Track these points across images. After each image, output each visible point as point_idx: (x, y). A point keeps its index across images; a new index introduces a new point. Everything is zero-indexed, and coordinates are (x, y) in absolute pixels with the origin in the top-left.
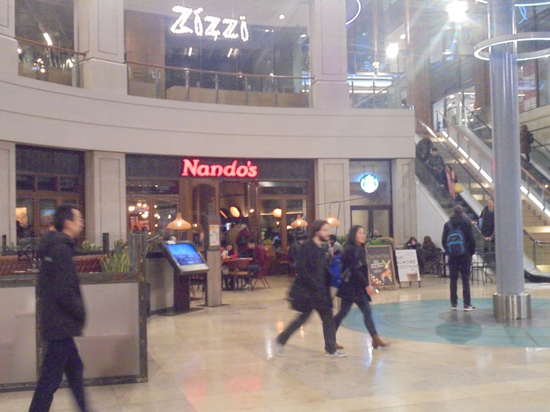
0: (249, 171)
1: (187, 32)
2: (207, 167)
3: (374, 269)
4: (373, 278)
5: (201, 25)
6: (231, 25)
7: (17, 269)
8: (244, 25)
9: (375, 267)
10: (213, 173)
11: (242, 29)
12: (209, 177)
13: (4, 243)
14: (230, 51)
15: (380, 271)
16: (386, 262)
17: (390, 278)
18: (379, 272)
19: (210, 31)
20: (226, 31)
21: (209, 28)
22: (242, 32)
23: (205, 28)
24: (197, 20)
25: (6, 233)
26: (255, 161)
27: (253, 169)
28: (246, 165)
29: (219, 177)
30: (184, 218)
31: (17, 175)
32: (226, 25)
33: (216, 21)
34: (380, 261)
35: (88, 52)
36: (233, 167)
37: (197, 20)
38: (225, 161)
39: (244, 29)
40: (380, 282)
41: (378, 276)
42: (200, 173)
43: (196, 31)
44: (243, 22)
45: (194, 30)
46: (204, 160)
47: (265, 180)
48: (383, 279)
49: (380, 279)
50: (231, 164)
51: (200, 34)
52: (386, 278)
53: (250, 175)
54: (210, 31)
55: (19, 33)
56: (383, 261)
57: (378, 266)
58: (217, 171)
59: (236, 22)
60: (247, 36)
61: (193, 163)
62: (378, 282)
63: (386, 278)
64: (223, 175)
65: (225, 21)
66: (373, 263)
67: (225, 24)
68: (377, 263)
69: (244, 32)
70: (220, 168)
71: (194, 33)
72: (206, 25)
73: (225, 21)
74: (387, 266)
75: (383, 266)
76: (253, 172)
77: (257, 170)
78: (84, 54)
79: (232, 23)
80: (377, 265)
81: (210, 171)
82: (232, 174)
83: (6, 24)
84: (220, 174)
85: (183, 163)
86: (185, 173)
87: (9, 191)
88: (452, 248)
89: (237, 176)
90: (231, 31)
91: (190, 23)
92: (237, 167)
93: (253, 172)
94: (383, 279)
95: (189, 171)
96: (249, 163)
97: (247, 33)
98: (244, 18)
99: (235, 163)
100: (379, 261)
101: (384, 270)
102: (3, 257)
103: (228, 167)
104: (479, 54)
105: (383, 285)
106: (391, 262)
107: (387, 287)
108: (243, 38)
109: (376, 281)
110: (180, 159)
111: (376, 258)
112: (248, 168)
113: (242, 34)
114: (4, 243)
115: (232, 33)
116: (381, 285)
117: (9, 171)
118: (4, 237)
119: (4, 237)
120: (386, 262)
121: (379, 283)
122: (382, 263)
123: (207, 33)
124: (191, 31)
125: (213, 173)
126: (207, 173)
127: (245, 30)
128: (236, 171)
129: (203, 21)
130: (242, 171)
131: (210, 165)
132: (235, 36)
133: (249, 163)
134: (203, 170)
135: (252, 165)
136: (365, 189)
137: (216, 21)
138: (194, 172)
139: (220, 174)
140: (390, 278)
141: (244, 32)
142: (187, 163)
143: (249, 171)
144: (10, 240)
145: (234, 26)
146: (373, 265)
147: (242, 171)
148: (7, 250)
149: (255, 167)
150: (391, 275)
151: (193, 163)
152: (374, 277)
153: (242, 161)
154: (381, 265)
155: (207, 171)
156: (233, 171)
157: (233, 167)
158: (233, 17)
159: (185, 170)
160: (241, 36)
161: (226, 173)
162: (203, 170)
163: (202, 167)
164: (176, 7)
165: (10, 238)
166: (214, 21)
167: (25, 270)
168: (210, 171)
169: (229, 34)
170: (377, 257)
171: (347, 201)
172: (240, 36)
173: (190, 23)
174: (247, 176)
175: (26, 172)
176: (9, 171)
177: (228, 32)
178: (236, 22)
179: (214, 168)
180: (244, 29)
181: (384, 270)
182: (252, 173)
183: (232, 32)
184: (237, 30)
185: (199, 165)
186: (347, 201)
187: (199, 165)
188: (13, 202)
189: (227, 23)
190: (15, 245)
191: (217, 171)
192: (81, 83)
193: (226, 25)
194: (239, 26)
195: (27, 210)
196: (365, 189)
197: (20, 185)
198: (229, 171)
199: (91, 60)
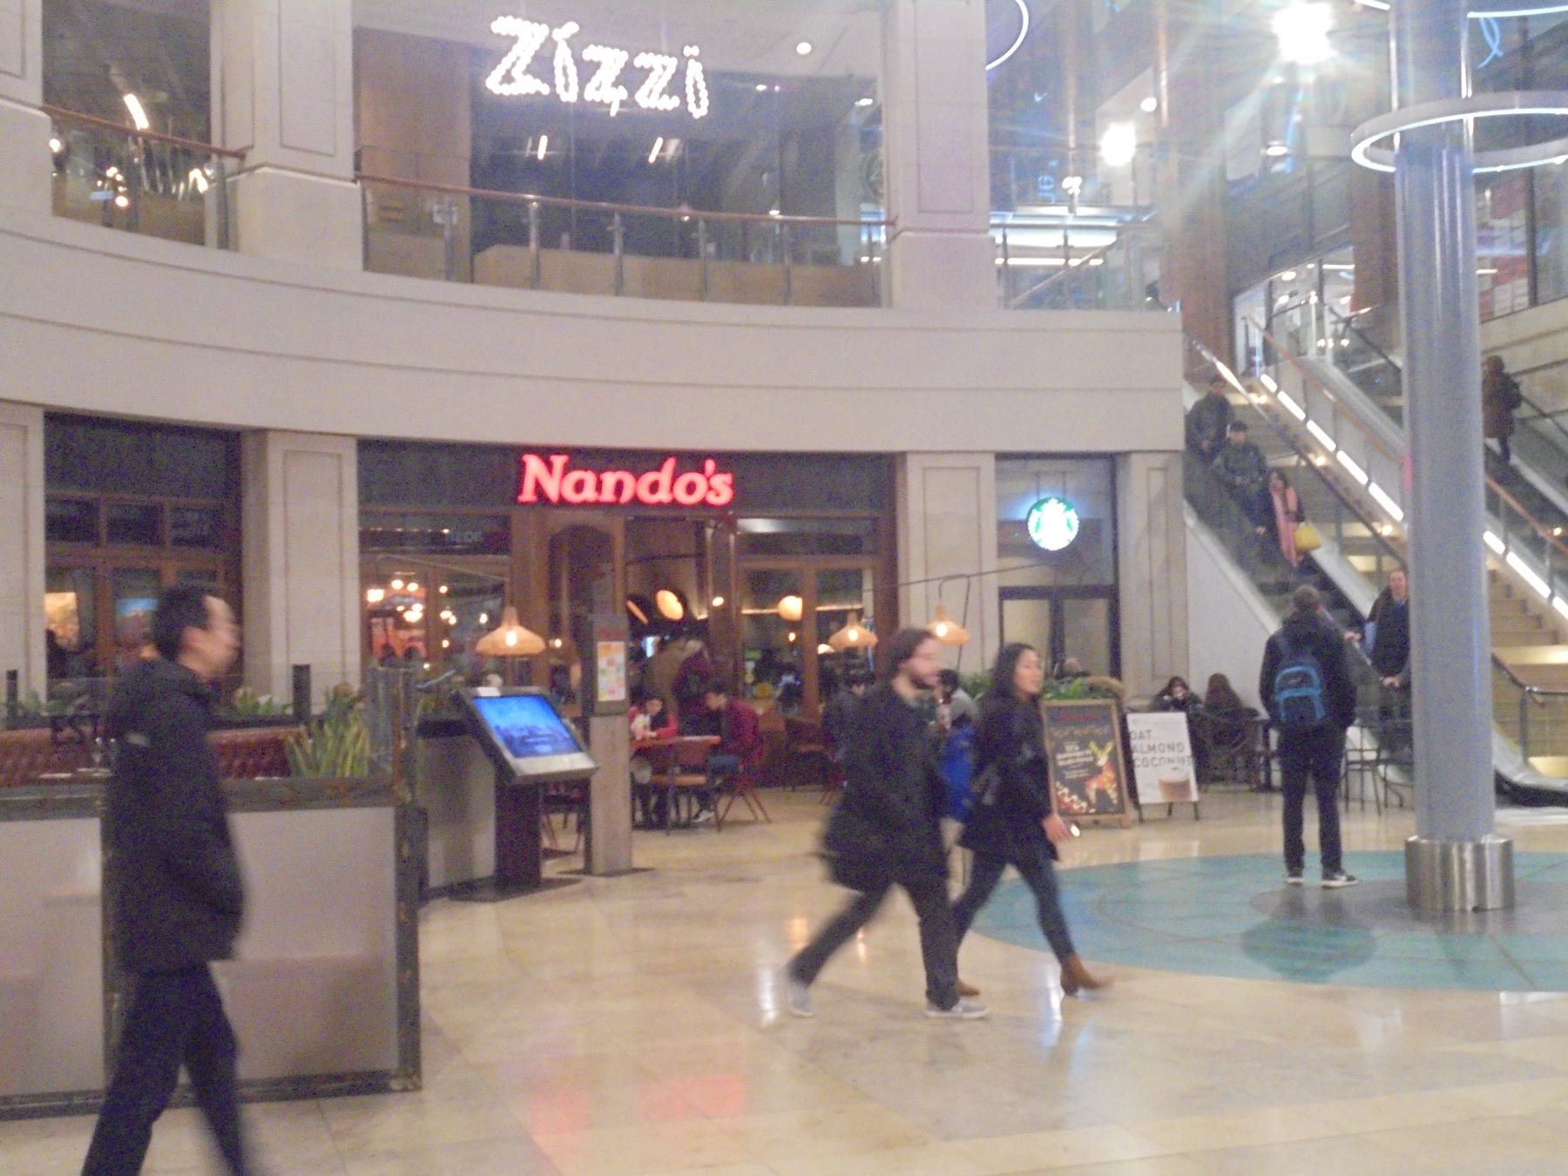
0: (710, 488)
1: (532, 92)
2: (589, 478)
3: (1066, 768)
5: (573, 71)
6: (658, 70)
7: (48, 767)
8: (695, 71)
9: (1070, 762)
10: (608, 495)
11: (689, 82)
12: (597, 504)
13: (12, 693)
14: (656, 144)
15: (1083, 773)
16: (1102, 747)
17: (1113, 795)
18: (1082, 775)
19: (598, 89)
20: (644, 90)
21: (595, 81)
22: (689, 90)
23: (583, 81)
24: (563, 57)
25: (17, 664)
26: (727, 461)
27: (722, 482)
28: (702, 471)
29: (625, 506)
31: (49, 500)
32: (645, 73)
33: (615, 61)
34: (1083, 744)
35: (251, 147)
36: (664, 477)
37: (563, 57)
38: (641, 460)
39: (695, 84)
40: (1084, 804)
41: (1078, 787)
42: (570, 495)
43: (560, 90)
44: (692, 63)
45: (553, 86)
46: (580, 457)
47: (755, 514)
48: (1092, 795)
49: (1083, 797)
50: (659, 469)
51: (569, 96)
52: (1101, 793)
53: (712, 499)
54: (598, 89)
55: (53, 95)
56: (1093, 745)
57: (1079, 760)
58: (619, 487)
59: (672, 63)
60: (705, 102)
61: (549, 466)
62: (1078, 805)
63: (1101, 793)
65: (642, 60)
66: (1063, 751)
67: (642, 68)
68: (1074, 751)
69: (696, 92)
70: (628, 479)
71: (554, 95)
72: (587, 71)
73: (642, 60)
74: (1103, 760)
75: (1091, 759)
76: (720, 490)
77: (733, 486)
78: (240, 155)
79: (661, 67)
80: (1075, 758)
81: (599, 487)
82: (663, 496)
83: (17, 69)
84: (626, 496)
85: (522, 466)
86: (528, 495)
87: (26, 545)
89: (674, 503)
90: (658, 89)
91: (542, 65)
92: (675, 478)
93: (720, 490)
94: (1092, 795)
95: (539, 488)
96: (710, 465)
97: (704, 94)
98: (695, 51)
99: (670, 465)
100: (1079, 744)
101: (1094, 770)
102: (9, 733)
103: (650, 477)
104: (1366, 154)
105: (1091, 814)
106: (1115, 749)
107: (1102, 818)
108: (692, 108)
109: (1072, 801)
110: (514, 455)
111: (1071, 738)
112: (708, 479)
113: (691, 98)
114: (12, 693)
115: (661, 94)
116: (1087, 813)
117: (26, 487)
118: (13, 675)
119: (13, 675)
120: (1102, 747)
121: (1081, 808)
122: (1088, 752)
123: (591, 94)
124: (545, 90)
125: (608, 495)
126: (589, 494)
127: (699, 86)
128: (672, 489)
129: (578, 61)
130: (691, 488)
131: (599, 472)
132: (671, 103)
133: (710, 465)
134: (579, 486)
135: (717, 471)
136: (1040, 540)
137: (615, 61)
138: (552, 490)
139: (626, 496)
140: (1113, 795)
141: (696, 92)
142: (534, 465)
143: (710, 488)
144: (28, 685)
145: (668, 76)
146: (1064, 756)
147: (691, 488)
148: (20, 713)
149: (727, 478)
150: (1114, 786)
151: (549, 466)
152: (1066, 790)
153: (691, 460)
154: (1085, 756)
155: (591, 488)
156: (664, 487)
157: (664, 477)
158: (665, 48)
159: (529, 485)
160: (687, 104)
161: (645, 495)
162: (579, 486)
163: (575, 476)
164: (501, 19)
165: (28, 679)
166: (611, 60)
167: (72, 771)
168: (599, 487)
169: (652, 97)
170: (1076, 733)
171: (990, 573)
172: (684, 102)
173: (542, 65)
174: (704, 503)
175: (74, 492)
176: (26, 487)
177: (651, 92)
178: (672, 63)
179: (610, 479)
180: (695, 84)
181: (1094, 770)
182: (718, 495)
183: (660, 90)
184: (676, 86)
185: (567, 470)
186: (990, 573)
187: (567, 470)
188: (38, 577)
189: (647, 66)
190: (43, 698)
191: (619, 487)
192: (231, 237)
193: (645, 73)
194: (680, 74)
195: (78, 599)
196: (1040, 540)
197: (58, 528)
198: (654, 487)
199: (259, 171)
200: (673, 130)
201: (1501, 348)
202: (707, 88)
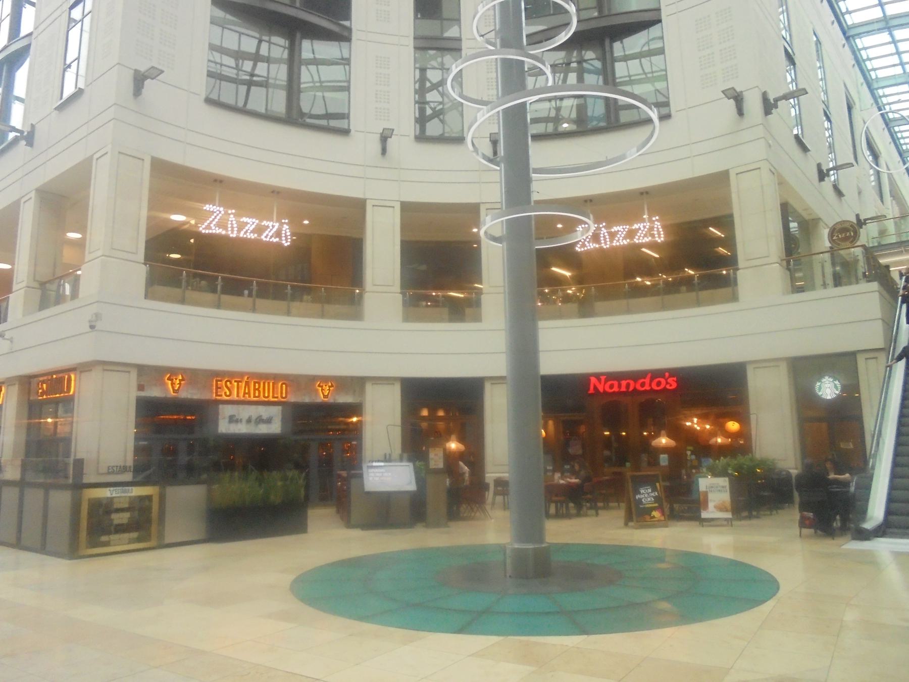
0: (667, 383)
4: (586, 506)
10: (623, 389)
12: (620, 393)
14: (5, 265)
29: (631, 392)
30: (669, 436)
42: (607, 389)
53: (668, 387)
58: (628, 385)
59: (277, 225)
64: (635, 389)
70: (632, 382)
72: (241, 226)
79: (272, 226)
81: (620, 386)
82: (647, 387)
88: (150, 535)
90: (270, 234)
95: (595, 388)
112: (666, 380)
124: (224, 232)
126: (615, 389)
128: (650, 385)
129: (238, 222)
134: (611, 387)
136: (86, 474)
139: (631, 389)
143: (667, 383)
145: (275, 230)
159: (592, 387)
161: (639, 387)
163: (610, 383)
168: (620, 386)
169: (267, 237)
178: (277, 225)
182: (671, 386)
184: (278, 234)
194: (651, 229)
196: (86, 474)
198: (643, 385)
200: (833, 248)
201: (90, 332)
202: (265, 232)
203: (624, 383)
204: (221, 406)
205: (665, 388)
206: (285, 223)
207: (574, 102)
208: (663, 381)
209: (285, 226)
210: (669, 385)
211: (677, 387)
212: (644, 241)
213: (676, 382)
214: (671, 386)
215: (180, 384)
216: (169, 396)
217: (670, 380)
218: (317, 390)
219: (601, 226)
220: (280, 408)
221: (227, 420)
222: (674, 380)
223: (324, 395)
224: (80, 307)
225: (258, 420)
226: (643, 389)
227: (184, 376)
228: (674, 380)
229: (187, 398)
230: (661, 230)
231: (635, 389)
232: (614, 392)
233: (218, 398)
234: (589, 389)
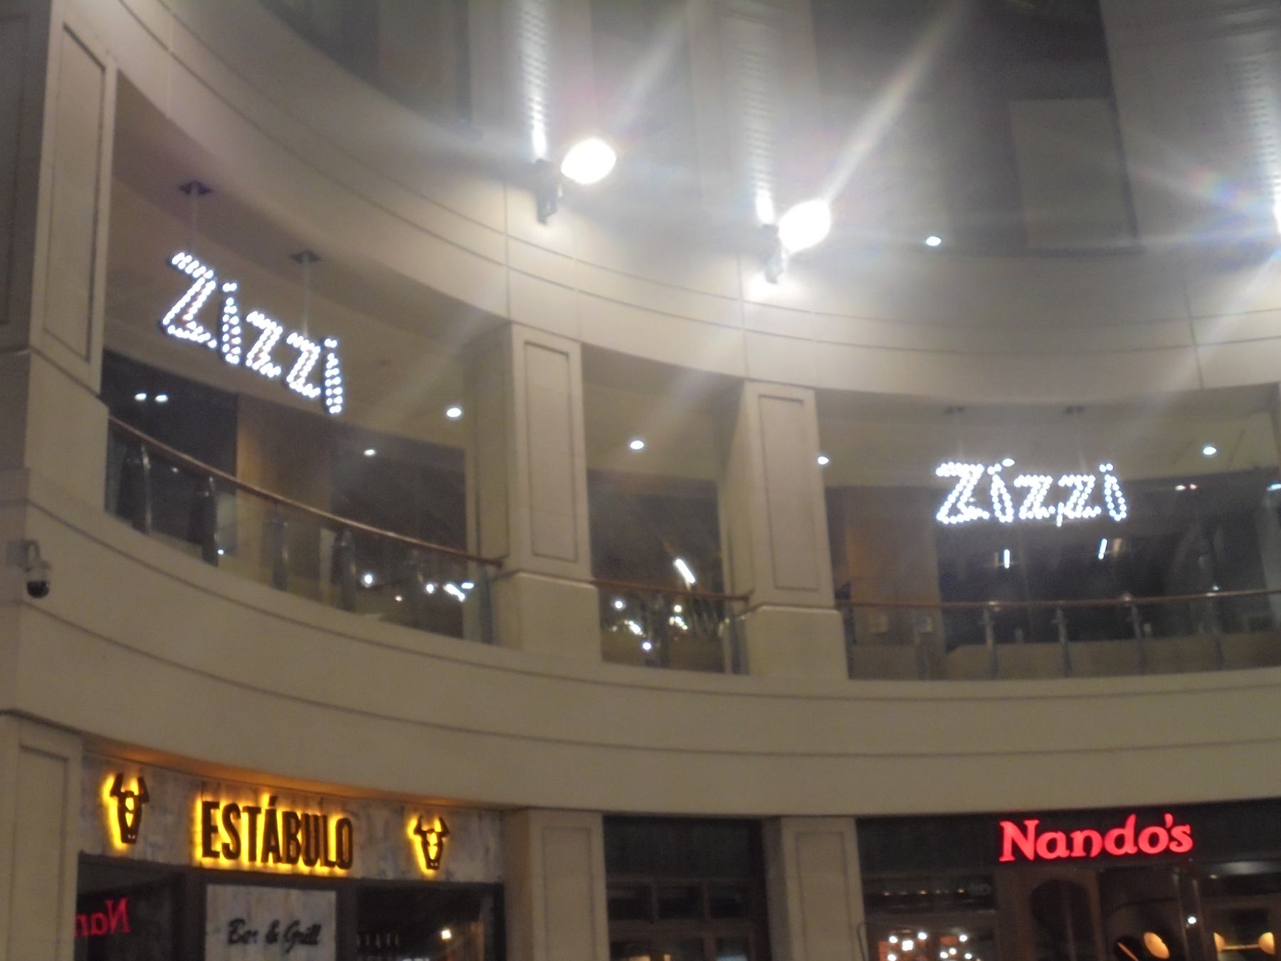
0: (1171, 839)
1: (975, 518)
2: (1060, 837)
5: (1007, 497)
8: (1111, 483)
10: (1078, 851)
11: (1108, 492)
19: (1030, 509)
21: (1027, 503)
22: (1109, 499)
24: (998, 486)
26: (1184, 813)
28: (1162, 824)
36: (1128, 832)
37: (998, 486)
42: (1044, 853)
43: (998, 514)
44: (1107, 477)
45: (992, 511)
46: (1052, 820)
50: (1122, 825)
51: (1007, 518)
53: (1174, 847)
54: (1030, 509)
58: (1088, 843)
59: (1091, 480)
60: (1123, 508)
61: (1024, 830)
64: (1104, 851)
69: (1115, 500)
70: (1095, 836)
73: (1065, 481)
76: (1182, 840)
79: (1081, 484)
81: (1070, 845)
82: (1129, 848)
84: (1095, 851)
85: (1001, 832)
86: (1007, 856)
89: (1140, 853)
91: (982, 495)
93: (1182, 840)
95: (1016, 848)
96: (1169, 818)
98: (1110, 467)
99: (1132, 820)
103: (1116, 832)
110: (988, 824)
112: (1169, 831)
113: (1111, 506)
115: (1085, 506)
123: (1024, 514)
125: (1078, 851)
126: (1061, 851)
128: (1136, 843)
129: (1010, 488)
130: (1154, 840)
133: (1169, 818)
134: (1052, 845)
135: (1175, 824)
138: (1028, 850)
139: (1095, 851)
142: (1010, 829)
143: (1171, 839)
145: (1089, 490)
147: (1154, 840)
149: (1187, 829)
151: (1024, 830)
153: (1150, 815)
157: (1128, 832)
159: (1007, 847)
160: (1108, 510)
162: (1052, 845)
163: (1048, 836)
168: (1070, 845)
172: (1105, 510)
173: (982, 495)
178: (1091, 480)
179: (1079, 837)
182: (1180, 844)
183: (1083, 503)
184: (1097, 498)
185: (1038, 833)
187: (1038, 833)
194: (1099, 488)
198: (1120, 842)
203: (1079, 837)
204: (211, 889)
205: (1167, 850)
206: (1108, 472)
207: (762, 188)
208: (1160, 831)
209: (1107, 477)
210: (1176, 843)
211: (1190, 851)
212: (1086, 515)
213: (1189, 835)
214: (1180, 844)
215: (440, 845)
216: (412, 876)
217: (1178, 832)
218: (408, 845)
219: (991, 470)
220: (332, 896)
221: (223, 936)
222: (1185, 833)
223: (429, 861)
224: (339, 634)
225: (290, 935)
226: (1121, 852)
227: (447, 824)
228: (1185, 833)
229: (385, 882)
230: (1119, 494)
231: (1104, 851)
232: (1058, 859)
233: (208, 862)
234: (1001, 853)
